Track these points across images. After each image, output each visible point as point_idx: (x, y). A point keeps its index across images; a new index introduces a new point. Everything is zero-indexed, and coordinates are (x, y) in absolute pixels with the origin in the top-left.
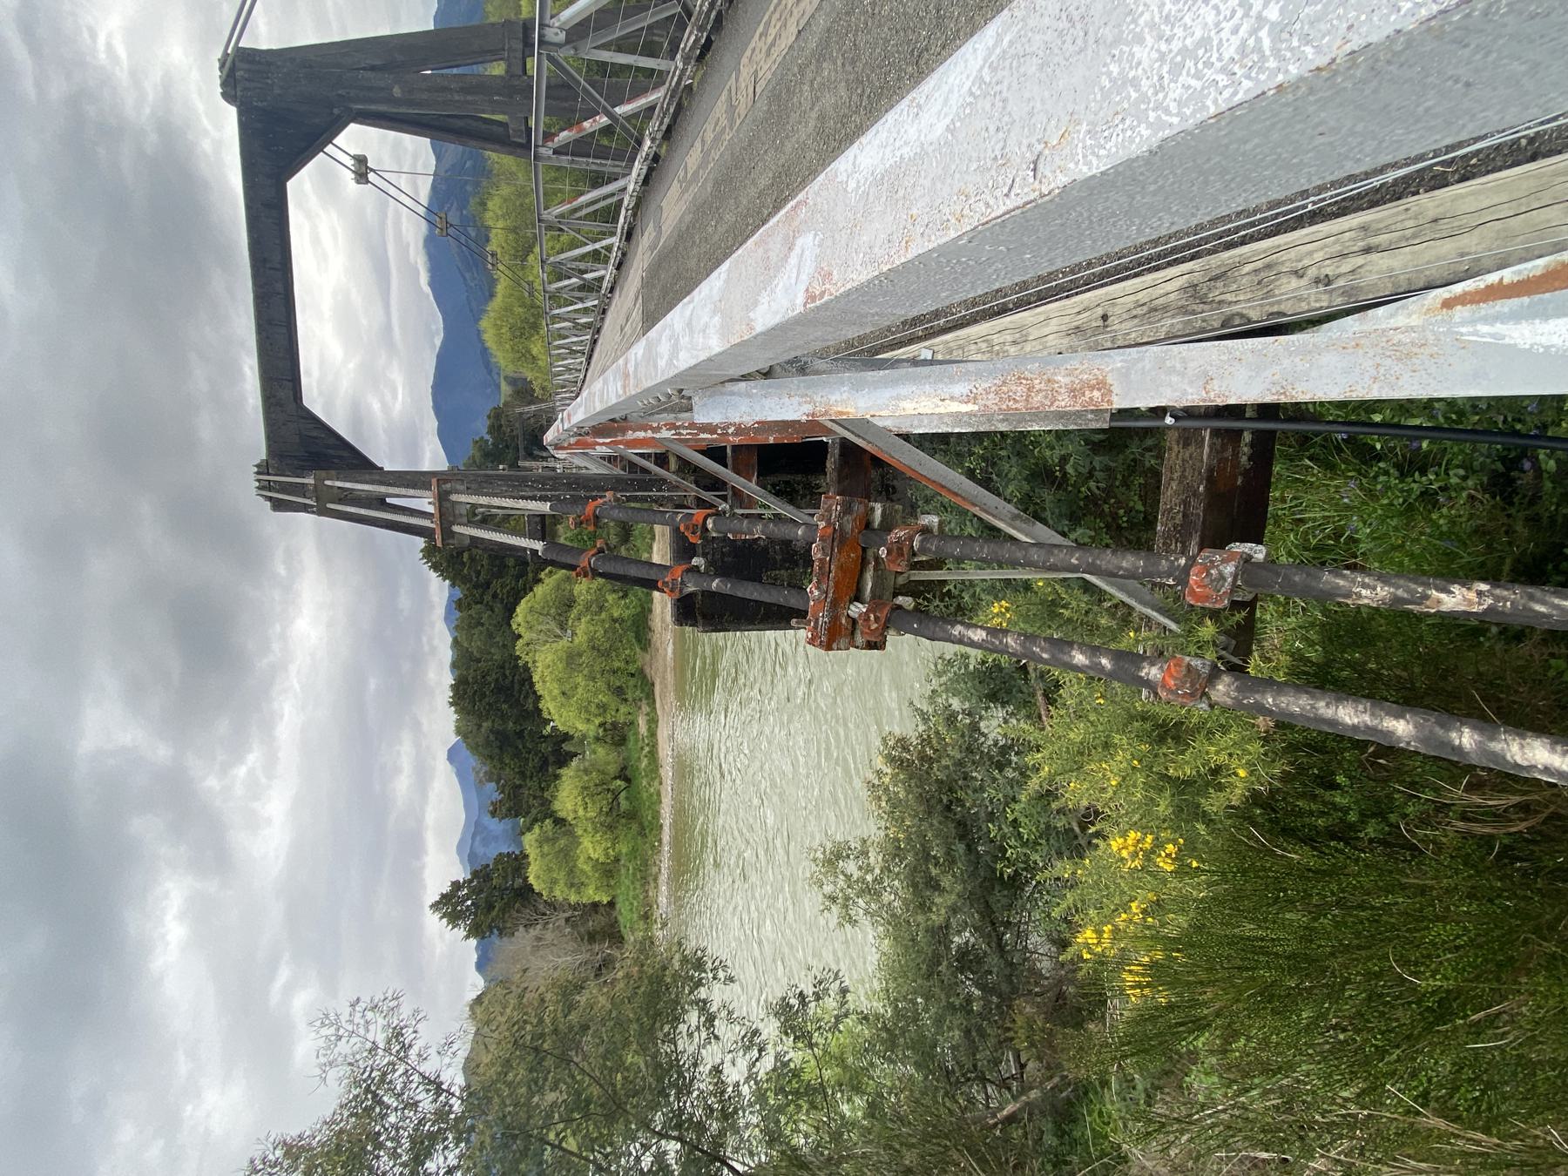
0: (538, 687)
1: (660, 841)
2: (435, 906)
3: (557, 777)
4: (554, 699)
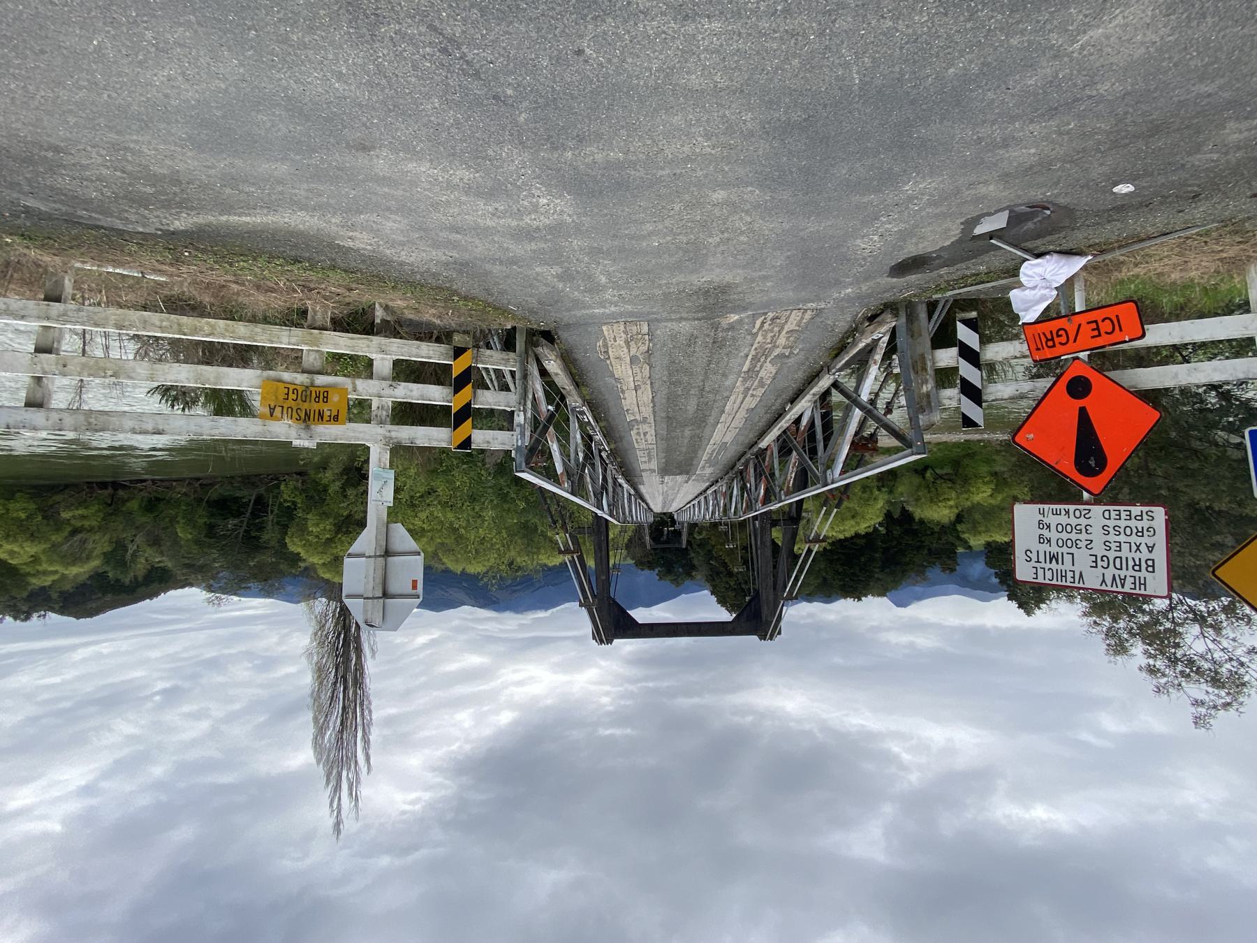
0: (848, 535)
1: (979, 441)
2: (1029, 613)
3: (922, 522)
4: (858, 524)
